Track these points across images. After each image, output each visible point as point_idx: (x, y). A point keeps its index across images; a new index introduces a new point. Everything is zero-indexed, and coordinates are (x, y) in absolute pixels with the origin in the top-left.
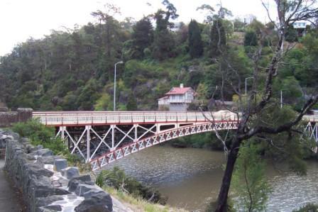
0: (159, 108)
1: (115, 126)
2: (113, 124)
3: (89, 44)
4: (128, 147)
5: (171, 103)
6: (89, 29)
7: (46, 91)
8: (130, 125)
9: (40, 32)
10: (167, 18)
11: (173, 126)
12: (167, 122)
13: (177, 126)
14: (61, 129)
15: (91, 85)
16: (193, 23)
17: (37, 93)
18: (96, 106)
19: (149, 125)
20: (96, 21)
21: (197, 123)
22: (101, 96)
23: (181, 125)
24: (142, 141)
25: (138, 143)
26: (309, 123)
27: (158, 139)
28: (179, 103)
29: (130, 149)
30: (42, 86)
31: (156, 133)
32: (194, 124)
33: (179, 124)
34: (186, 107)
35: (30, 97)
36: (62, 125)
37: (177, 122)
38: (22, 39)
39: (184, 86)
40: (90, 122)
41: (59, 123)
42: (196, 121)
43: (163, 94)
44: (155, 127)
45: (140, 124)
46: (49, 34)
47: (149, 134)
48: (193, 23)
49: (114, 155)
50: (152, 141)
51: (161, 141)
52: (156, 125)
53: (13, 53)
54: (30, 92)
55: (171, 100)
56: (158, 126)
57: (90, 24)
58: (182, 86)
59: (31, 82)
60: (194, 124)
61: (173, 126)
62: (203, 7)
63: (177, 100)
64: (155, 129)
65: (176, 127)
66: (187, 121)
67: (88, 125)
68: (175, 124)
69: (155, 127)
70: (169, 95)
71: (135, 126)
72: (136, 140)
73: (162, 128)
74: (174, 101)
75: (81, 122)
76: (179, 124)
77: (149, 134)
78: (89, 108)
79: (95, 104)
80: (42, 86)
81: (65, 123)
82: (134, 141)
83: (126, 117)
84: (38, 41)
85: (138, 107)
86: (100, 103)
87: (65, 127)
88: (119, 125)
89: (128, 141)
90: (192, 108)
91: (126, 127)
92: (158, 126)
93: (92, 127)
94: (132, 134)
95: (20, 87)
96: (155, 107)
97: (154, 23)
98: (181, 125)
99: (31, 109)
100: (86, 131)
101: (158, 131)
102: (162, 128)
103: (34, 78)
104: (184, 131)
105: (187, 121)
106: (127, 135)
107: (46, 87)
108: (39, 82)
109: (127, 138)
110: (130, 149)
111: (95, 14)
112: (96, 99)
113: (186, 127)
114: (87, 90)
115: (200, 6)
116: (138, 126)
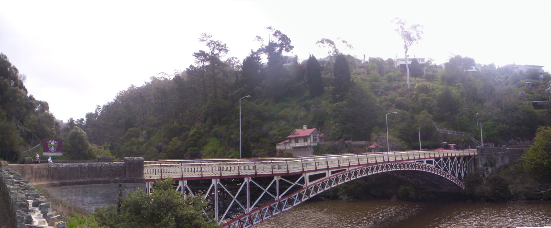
0: (278, 154)
3: (193, 86)
5: (294, 148)
6: (191, 72)
7: (149, 138)
8: (270, 178)
9: (140, 80)
12: (316, 170)
13: (329, 174)
14: (180, 183)
15: (198, 129)
16: (312, 59)
17: (141, 139)
18: (205, 152)
20: (145, 85)
21: (351, 169)
22: (209, 142)
23: (332, 173)
24: (287, 199)
27: (308, 193)
28: (304, 147)
30: (144, 132)
31: (304, 186)
32: (347, 169)
33: (330, 171)
34: (312, 150)
35: (133, 144)
36: (182, 179)
37: (328, 169)
38: (124, 87)
39: (308, 128)
40: (218, 174)
41: (178, 176)
42: (349, 166)
43: (284, 137)
44: (303, 178)
45: (283, 176)
46: (150, 81)
47: (297, 189)
48: (312, 59)
49: (250, 218)
50: (300, 197)
51: (311, 196)
52: (304, 175)
53: (116, 101)
54: (134, 139)
55: (294, 144)
57: (191, 66)
58: (305, 127)
59: (134, 129)
61: (324, 175)
62: (322, 42)
63: (301, 144)
64: (302, 181)
65: (327, 176)
66: (339, 167)
67: (215, 178)
68: (326, 172)
69: (303, 178)
70: (290, 139)
71: (276, 178)
72: (278, 197)
73: (312, 178)
74: (298, 145)
75: (206, 175)
76: (330, 171)
77: (297, 189)
78: (196, 155)
79: (203, 150)
80: (144, 132)
81: (187, 175)
83: (232, 167)
84: (140, 89)
85: (253, 152)
86: (208, 148)
87: (186, 182)
88: (256, 178)
89: (267, 199)
90: (317, 151)
91: (264, 180)
93: (253, 179)
94: (273, 190)
95: (124, 134)
96: (272, 153)
97: (264, 59)
99: (142, 158)
100: (213, 187)
101: (308, 183)
102: (312, 178)
103: (137, 124)
104: (337, 180)
105: (339, 167)
107: (150, 134)
108: (142, 129)
110: (271, 209)
112: (204, 145)
114: (193, 135)
115: (320, 40)
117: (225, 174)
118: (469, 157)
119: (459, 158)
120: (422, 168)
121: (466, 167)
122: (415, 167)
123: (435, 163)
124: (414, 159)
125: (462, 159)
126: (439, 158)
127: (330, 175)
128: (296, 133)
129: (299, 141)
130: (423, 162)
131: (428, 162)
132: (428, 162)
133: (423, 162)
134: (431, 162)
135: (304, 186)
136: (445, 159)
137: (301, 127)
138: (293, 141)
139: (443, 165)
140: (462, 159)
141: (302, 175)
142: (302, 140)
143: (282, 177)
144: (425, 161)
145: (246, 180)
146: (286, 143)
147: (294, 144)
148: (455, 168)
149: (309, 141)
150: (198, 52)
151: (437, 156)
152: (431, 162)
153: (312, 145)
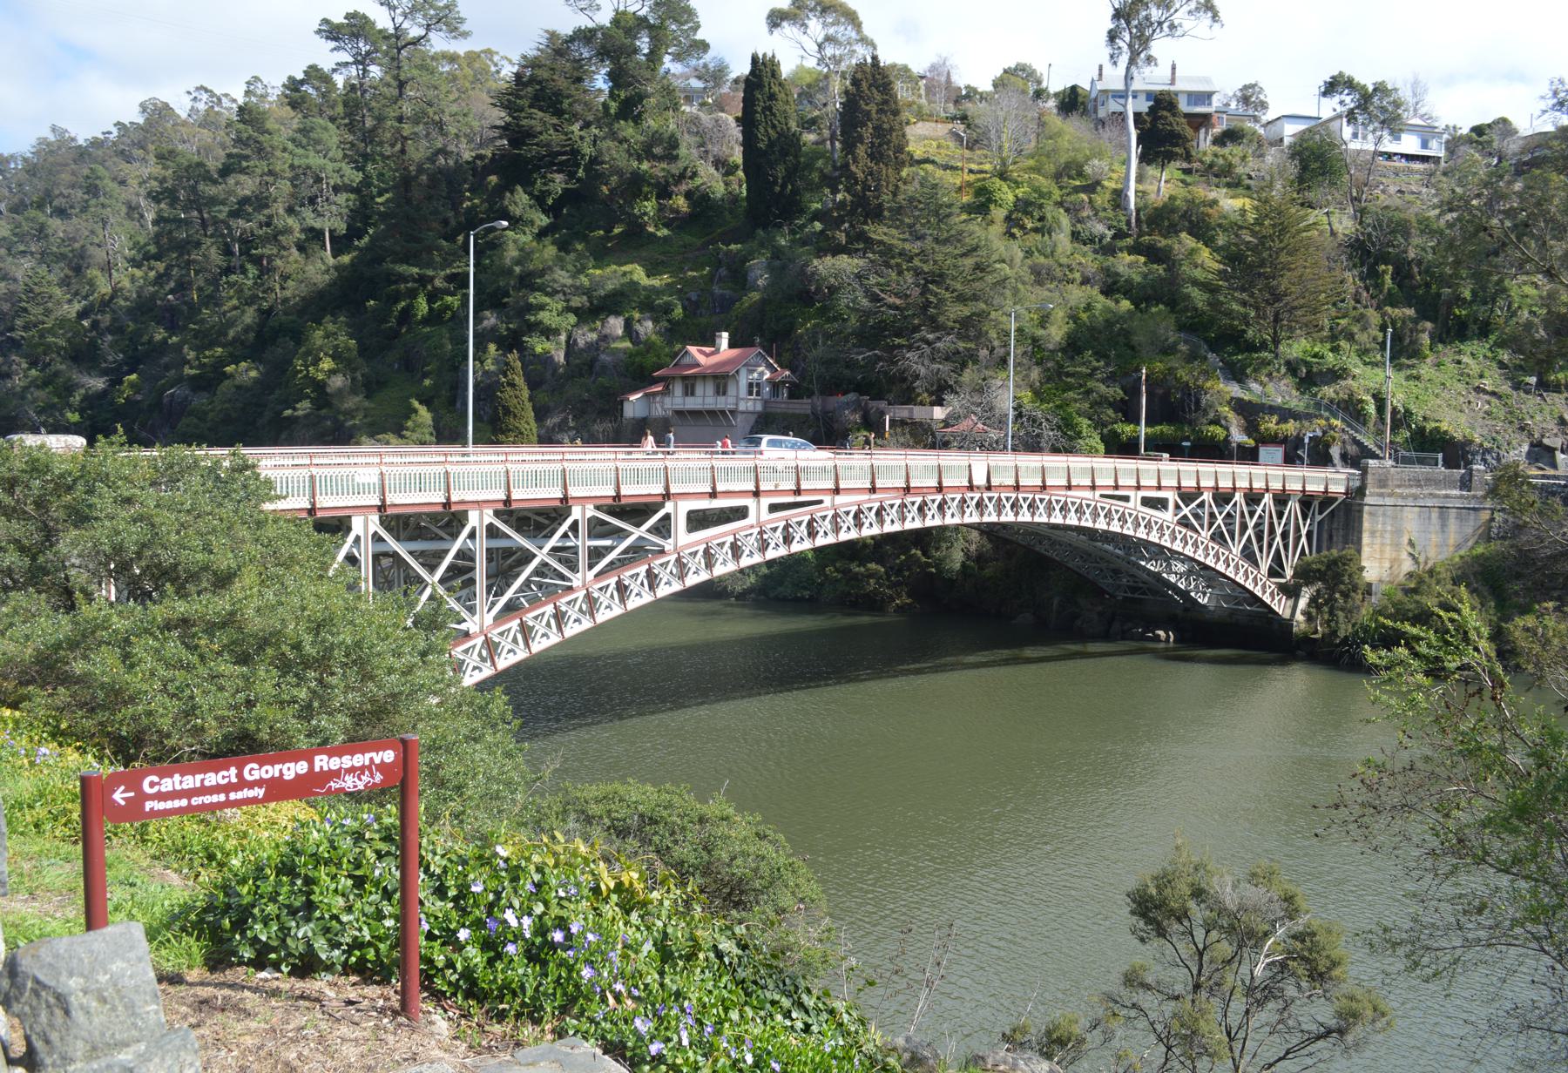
1: (489, 517)
2: (479, 504)
4: (642, 569)
5: (680, 413)
10: (654, 57)
11: (741, 513)
12: (713, 495)
13: (759, 511)
19: (637, 512)
21: (839, 499)
23: (774, 508)
24: (612, 581)
25: (494, 635)
26: (1238, 497)
28: (712, 413)
29: (652, 578)
33: (766, 502)
39: (731, 345)
42: (837, 491)
49: (589, 598)
52: (669, 507)
55: (678, 400)
56: (679, 511)
60: (827, 499)
61: (741, 513)
63: (704, 398)
64: (664, 528)
68: (749, 502)
69: (667, 517)
71: (576, 513)
73: (698, 520)
74: (692, 403)
76: (766, 502)
77: (638, 552)
82: (576, 580)
88: (508, 512)
91: (538, 521)
92: (679, 511)
93: (497, 514)
94: (461, 572)
98: (774, 508)
101: (682, 537)
102: (698, 520)
105: (798, 492)
106: (542, 556)
109: (543, 570)
111: (331, 32)
113: (803, 515)
116: (591, 512)
117: (399, 498)
118: (1327, 500)
119: (1281, 499)
120: (1122, 519)
121: (1285, 535)
122: (1095, 515)
123: (1177, 507)
124: (1093, 487)
125: (1293, 506)
126: (1199, 490)
127: (765, 515)
128: (687, 360)
129: (699, 390)
130: (1126, 499)
131: (1147, 502)
132: (1147, 502)
133: (1126, 499)
134: (1160, 504)
135: (668, 545)
136: (1222, 498)
137: (708, 340)
138: (678, 389)
139: (1212, 515)
140: (1293, 506)
141: (662, 505)
142: (710, 388)
143: (598, 508)
144: (1136, 497)
145: (473, 519)
146: (655, 394)
147: (678, 400)
148: (1272, 531)
149: (731, 390)
150: (338, 18)
151: (1189, 483)
152: (1160, 504)
153: (742, 407)
